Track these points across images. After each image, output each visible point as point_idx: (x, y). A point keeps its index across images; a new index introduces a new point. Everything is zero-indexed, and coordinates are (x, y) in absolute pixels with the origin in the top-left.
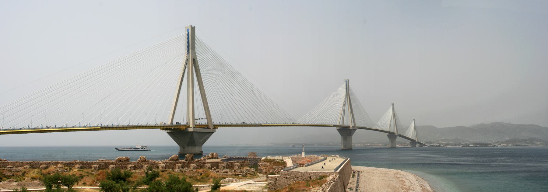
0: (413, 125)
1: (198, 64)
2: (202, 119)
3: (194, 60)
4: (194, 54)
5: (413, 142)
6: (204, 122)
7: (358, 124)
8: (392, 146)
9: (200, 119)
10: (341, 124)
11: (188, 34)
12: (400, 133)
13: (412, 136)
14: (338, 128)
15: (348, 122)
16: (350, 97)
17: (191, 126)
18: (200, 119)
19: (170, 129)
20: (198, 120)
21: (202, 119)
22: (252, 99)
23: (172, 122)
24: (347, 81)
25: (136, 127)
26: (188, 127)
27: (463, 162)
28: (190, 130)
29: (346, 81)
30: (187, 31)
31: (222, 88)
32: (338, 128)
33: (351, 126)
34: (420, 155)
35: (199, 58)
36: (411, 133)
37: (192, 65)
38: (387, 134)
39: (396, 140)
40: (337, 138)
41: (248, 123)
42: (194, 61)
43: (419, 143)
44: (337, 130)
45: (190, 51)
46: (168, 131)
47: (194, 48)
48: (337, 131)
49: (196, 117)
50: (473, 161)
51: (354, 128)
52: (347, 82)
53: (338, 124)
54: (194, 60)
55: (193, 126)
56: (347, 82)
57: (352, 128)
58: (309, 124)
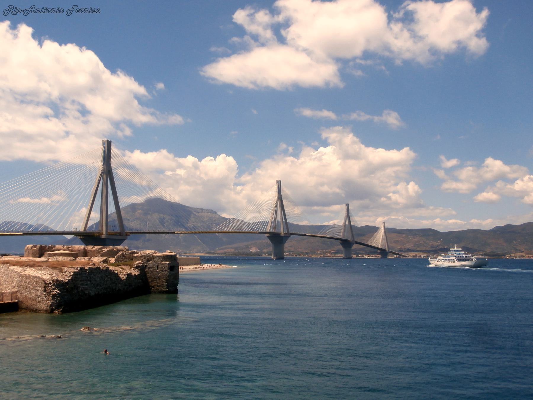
5: (383, 252)
6: (118, 230)
10: (271, 231)
12: (357, 240)
13: (382, 245)
14: (268, 235)
17: (104, 233)
19: (83, 236)
22: (62, 179)
23: (85, 229)
24: (279, 182)
25: (265, 259)
26: (102, 234)
27: (448, 351)
28: (103, 237)
32: (268, 235)
40: (269, 249)
46: (82, 237)
50: (326, 295)
51: (288, 235)
52: (279, 183)
55: (106, 233)
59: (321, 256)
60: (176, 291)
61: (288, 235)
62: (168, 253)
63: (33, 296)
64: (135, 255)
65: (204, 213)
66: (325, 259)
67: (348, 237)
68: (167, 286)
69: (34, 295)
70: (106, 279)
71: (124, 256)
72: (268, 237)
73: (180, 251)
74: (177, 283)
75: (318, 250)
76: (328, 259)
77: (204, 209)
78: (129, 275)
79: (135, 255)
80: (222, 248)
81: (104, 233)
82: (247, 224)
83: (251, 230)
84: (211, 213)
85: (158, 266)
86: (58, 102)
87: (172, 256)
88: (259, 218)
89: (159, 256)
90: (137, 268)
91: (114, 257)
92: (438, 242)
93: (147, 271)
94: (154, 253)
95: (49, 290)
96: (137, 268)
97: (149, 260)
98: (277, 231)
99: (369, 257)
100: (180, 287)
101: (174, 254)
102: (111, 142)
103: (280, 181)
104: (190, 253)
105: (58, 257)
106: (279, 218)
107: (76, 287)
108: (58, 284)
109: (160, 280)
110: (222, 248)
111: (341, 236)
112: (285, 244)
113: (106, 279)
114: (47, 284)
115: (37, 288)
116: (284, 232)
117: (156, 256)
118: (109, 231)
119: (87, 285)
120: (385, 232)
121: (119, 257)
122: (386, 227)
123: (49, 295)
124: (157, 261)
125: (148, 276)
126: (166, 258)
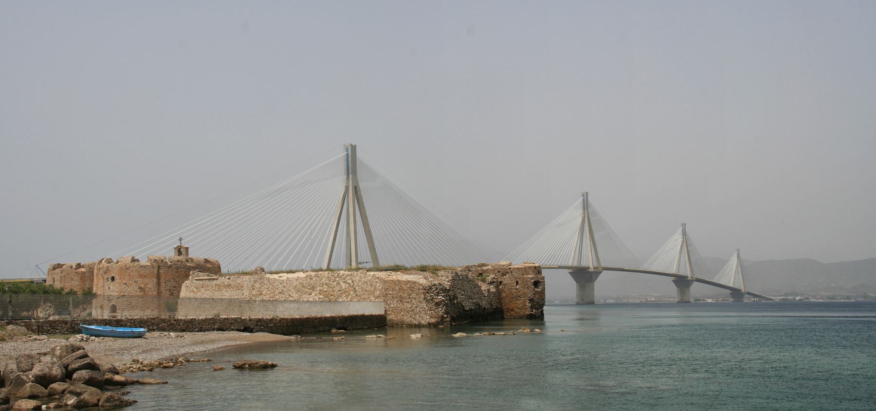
0: (734, 261)
1: (360, 192)
2: (367, 262)
3: (355, 187)
4: (355, 180)
5: (736, 293)
7: (604, 264)
8: (583, 299)
9: (364, 263)
10: (575, 264)
11: (347, 155)
13: (734, 283)
14: (570, 271)
15: (589, 262)
16: (591, 218)
18: (364, 263)
20: (361, 264)
21: (367, 262)
29: (583, 195)
30: (345, 151)
31: (403, 222)
32: (570, 271)
33: (591, 267)
34: (721, 319)
35: (362, 185)
36: (730, 276)
37: (353, 195)
38: (673, 278)
39: (689, 290)
40: (671, 291)
41: (408, 266)
42: (356, 189)
43: (749, 293)
44: (570, 273)
45: (351, 176)
47: (355, 173)
48: (569, 274)
49: (359, 260)
51: (597, 270)
52: (585, 196)
53: (570, 264)
54: (355, 187)
56: (585, 196)
57: (592, 270)
58: (545, 265)
60: (541, 316)
61: (597, 273)
63: (408, 306)
64: (485, 268)
67: (686, 271)
74: (543, 305)
79: (485, 268)
86: (84, 292)
88: (552, 248)
93: (502, 289)
95: (429, 298)
97: (503, 275)
98: (584, 264)
99: (713, 301)
103: (587, 193)
109: (520, 300)
111: (673, 271)
112: (596, 283)
114: (428, 290)
116: (593, 266)
117: (515, 268)
123: (431, 304)
124: (515, 275)
125: (504, 295)
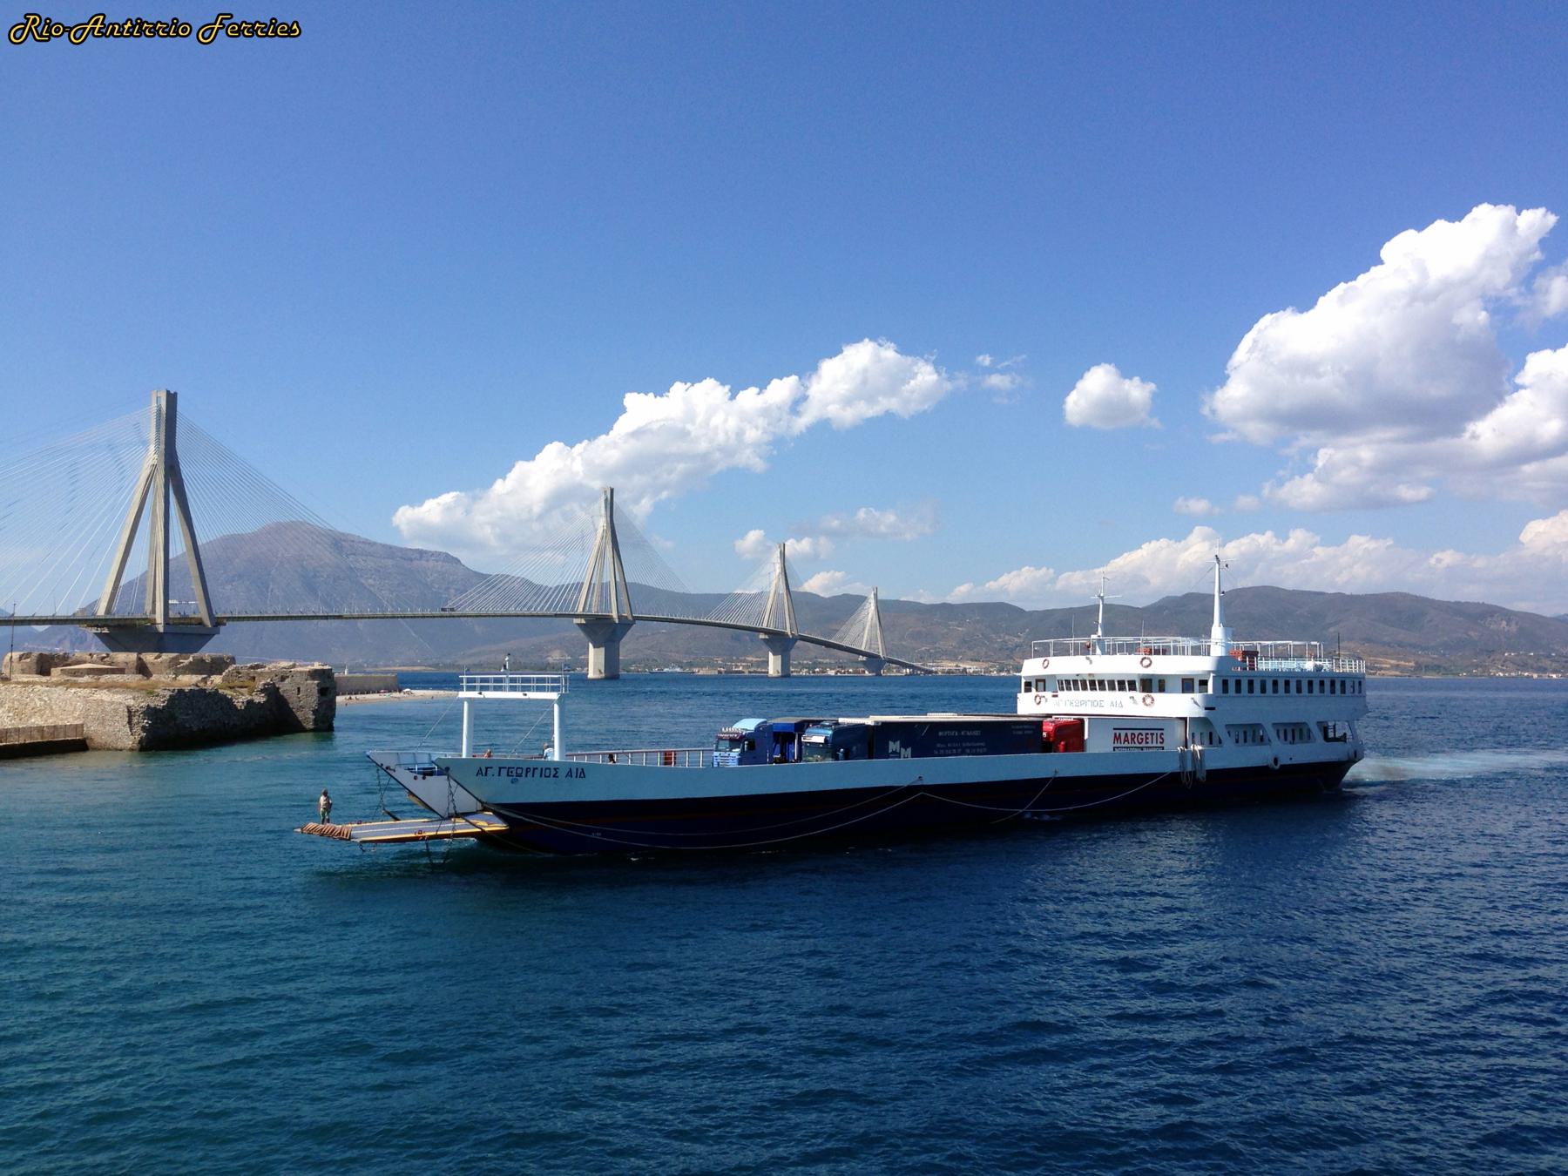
5: (873, 661)
59: (720, 672)
60: (331, 728)
61: (625, 625)
62: (317, 666)
65: (428, 561)
66: (732, 678)
68: (315, 720)
69: (111, 729)
70: (215, 706)
71: (239, 673)
72: (580, 625)
73: (361, 660)
75: (719, 655)
76: (739, 677)
77: (426, 552)
78: (250, 702)
80: (473, 651)
81: (159, 618)
82: (539, 590)
83: (542, 609)
84: (444, 561)
85: (299, 689)
87: (324, 671)
89: (301, 672)
90: (262, 691)
91: (221, 674)
92: (1019, 637)
94: (294, 666)
96: (262, 691)
97: (283, 679)
100: (336, 723)
101: (327, 667)
102: (176, 394)
103: (612, 491)
104: (386, 666)
105: (114, 676)
106: (609, 577)
107: (173, 717)
108: (151, 712)
110: (473, 651)
113: (215, 706)
115: (117, 718)
118: (171, 615)
119: (188, 714)
120: (877, 607)
121: (230, 674)
122: (879, 598)
124: (298, 680)
126: (314, 674)
